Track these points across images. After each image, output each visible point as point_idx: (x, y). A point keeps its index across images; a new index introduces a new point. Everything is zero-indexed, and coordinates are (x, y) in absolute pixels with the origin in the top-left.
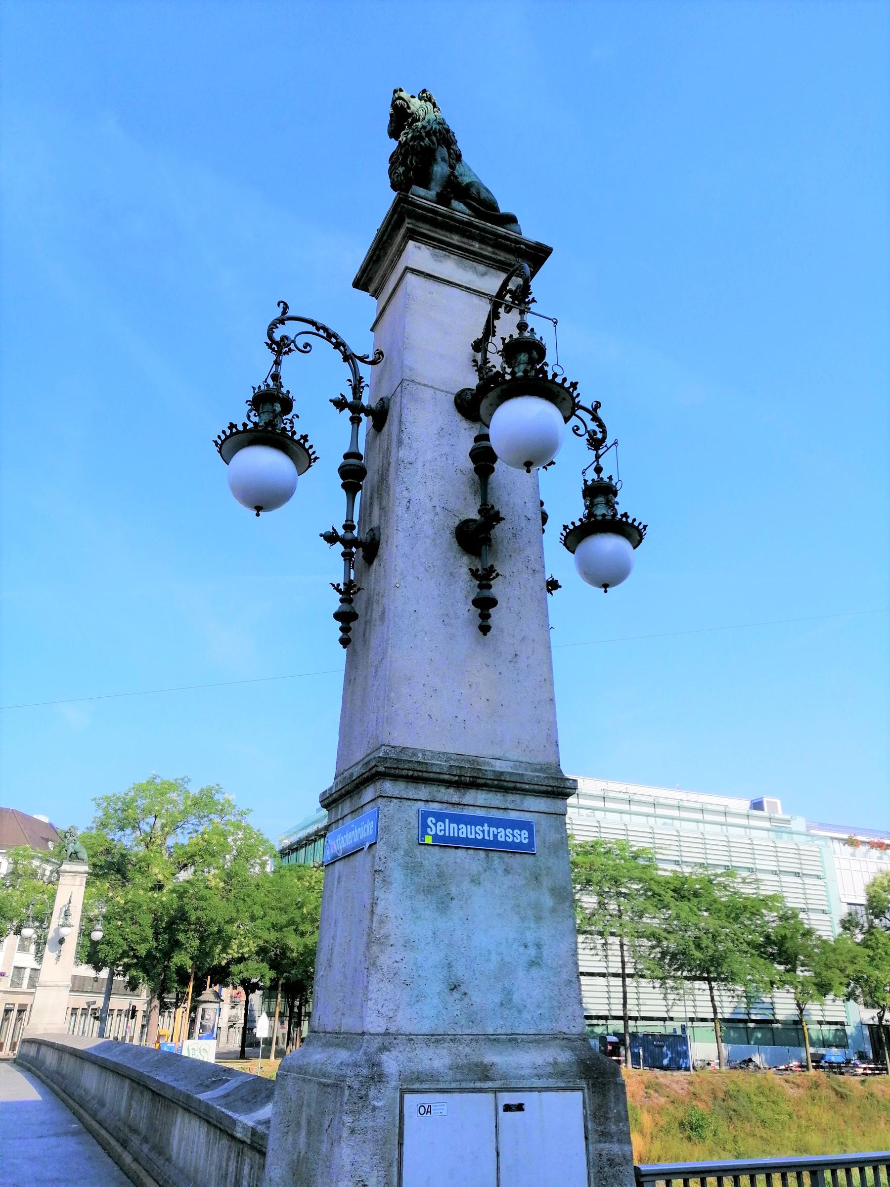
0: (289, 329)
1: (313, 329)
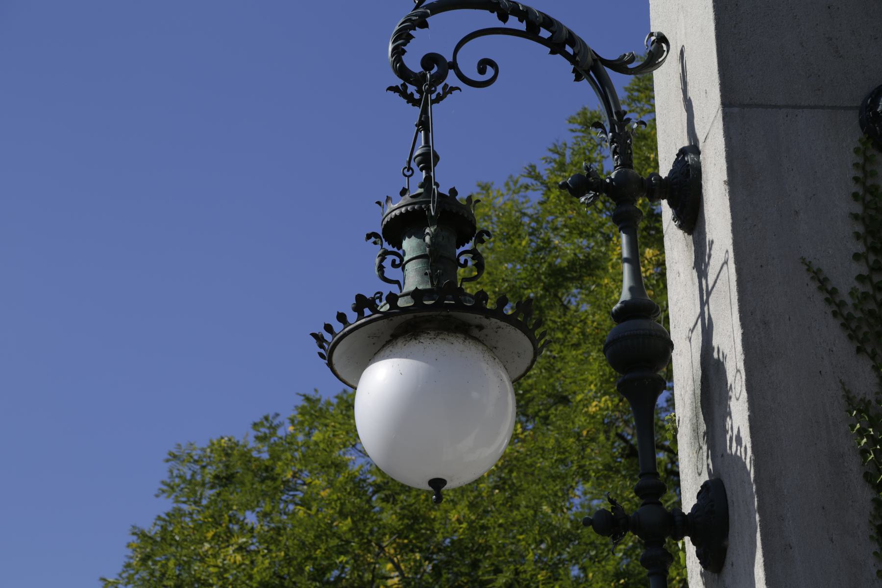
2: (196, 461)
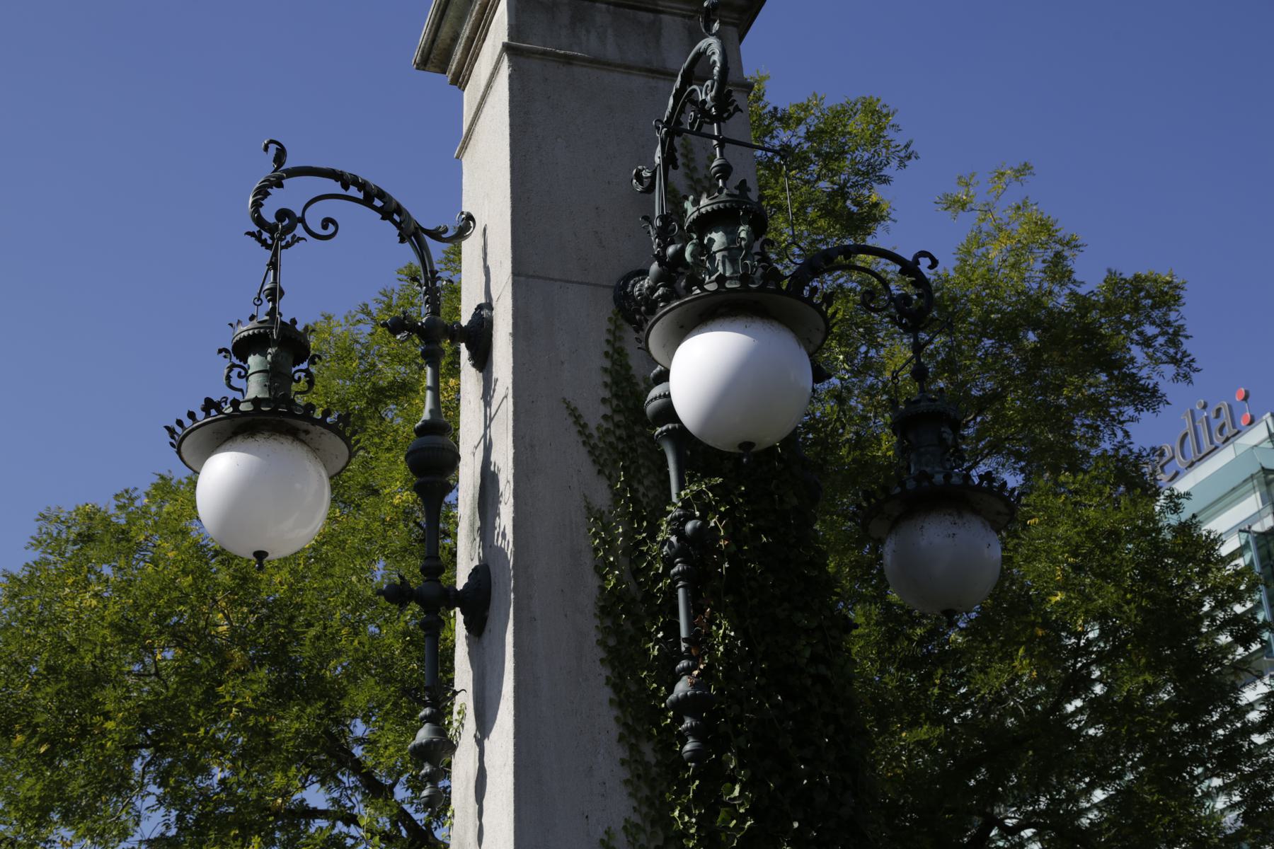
0: (292, 195)
1: (335, 187)
2: (62, 522)
